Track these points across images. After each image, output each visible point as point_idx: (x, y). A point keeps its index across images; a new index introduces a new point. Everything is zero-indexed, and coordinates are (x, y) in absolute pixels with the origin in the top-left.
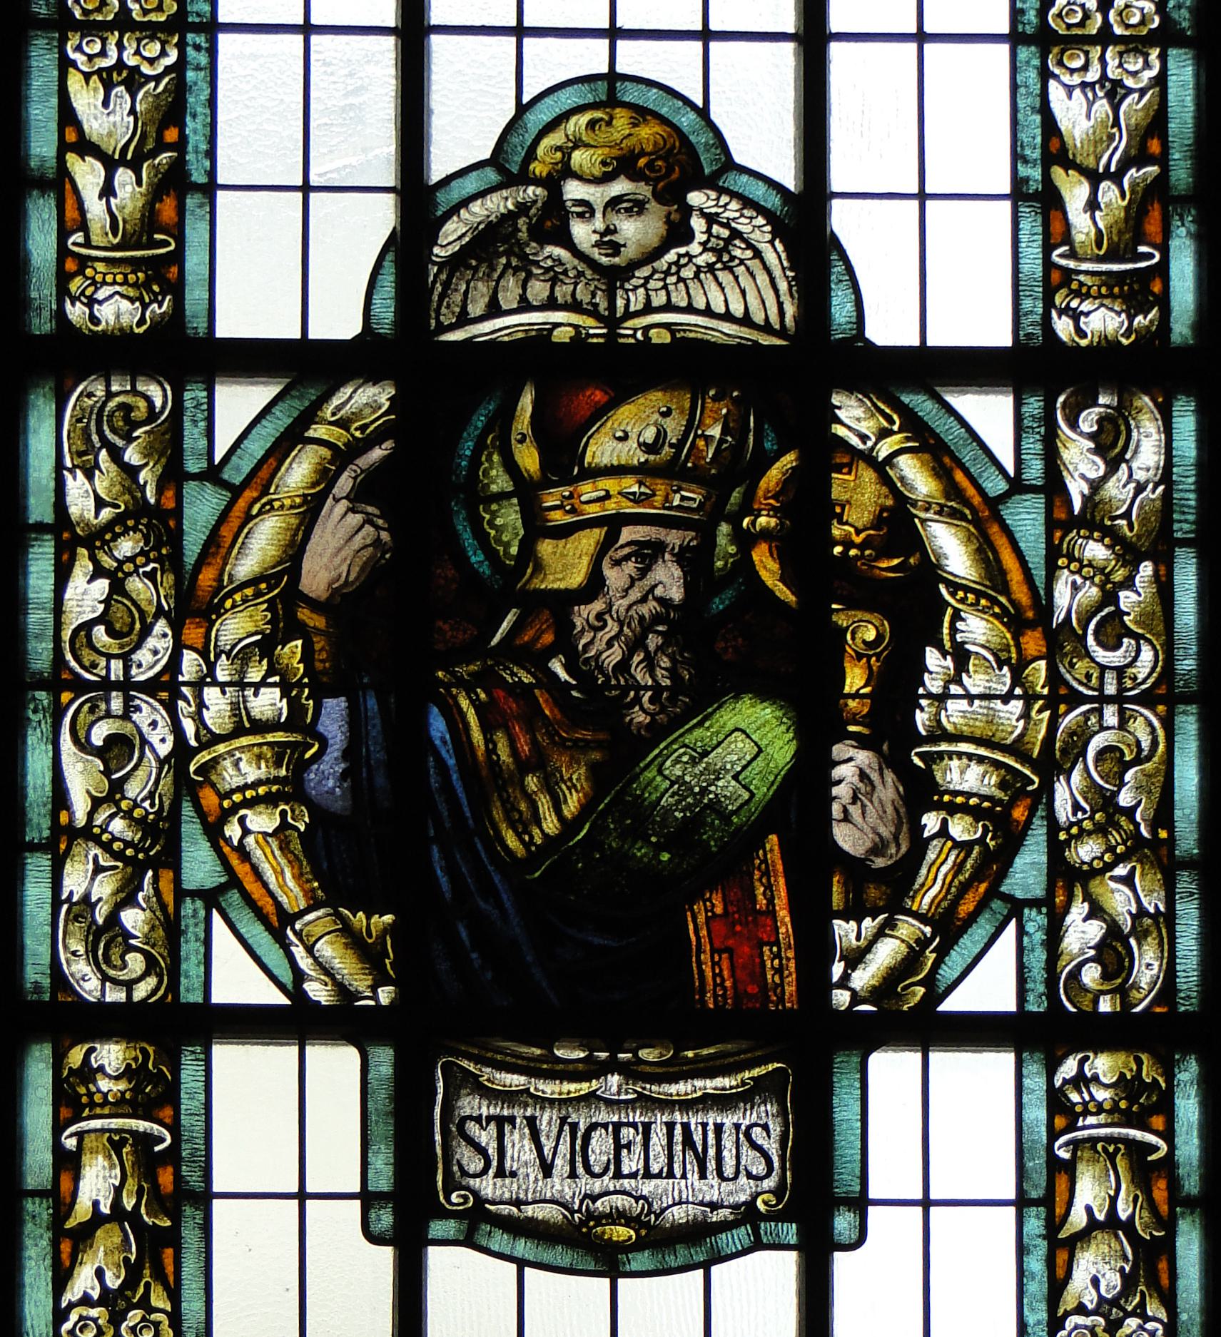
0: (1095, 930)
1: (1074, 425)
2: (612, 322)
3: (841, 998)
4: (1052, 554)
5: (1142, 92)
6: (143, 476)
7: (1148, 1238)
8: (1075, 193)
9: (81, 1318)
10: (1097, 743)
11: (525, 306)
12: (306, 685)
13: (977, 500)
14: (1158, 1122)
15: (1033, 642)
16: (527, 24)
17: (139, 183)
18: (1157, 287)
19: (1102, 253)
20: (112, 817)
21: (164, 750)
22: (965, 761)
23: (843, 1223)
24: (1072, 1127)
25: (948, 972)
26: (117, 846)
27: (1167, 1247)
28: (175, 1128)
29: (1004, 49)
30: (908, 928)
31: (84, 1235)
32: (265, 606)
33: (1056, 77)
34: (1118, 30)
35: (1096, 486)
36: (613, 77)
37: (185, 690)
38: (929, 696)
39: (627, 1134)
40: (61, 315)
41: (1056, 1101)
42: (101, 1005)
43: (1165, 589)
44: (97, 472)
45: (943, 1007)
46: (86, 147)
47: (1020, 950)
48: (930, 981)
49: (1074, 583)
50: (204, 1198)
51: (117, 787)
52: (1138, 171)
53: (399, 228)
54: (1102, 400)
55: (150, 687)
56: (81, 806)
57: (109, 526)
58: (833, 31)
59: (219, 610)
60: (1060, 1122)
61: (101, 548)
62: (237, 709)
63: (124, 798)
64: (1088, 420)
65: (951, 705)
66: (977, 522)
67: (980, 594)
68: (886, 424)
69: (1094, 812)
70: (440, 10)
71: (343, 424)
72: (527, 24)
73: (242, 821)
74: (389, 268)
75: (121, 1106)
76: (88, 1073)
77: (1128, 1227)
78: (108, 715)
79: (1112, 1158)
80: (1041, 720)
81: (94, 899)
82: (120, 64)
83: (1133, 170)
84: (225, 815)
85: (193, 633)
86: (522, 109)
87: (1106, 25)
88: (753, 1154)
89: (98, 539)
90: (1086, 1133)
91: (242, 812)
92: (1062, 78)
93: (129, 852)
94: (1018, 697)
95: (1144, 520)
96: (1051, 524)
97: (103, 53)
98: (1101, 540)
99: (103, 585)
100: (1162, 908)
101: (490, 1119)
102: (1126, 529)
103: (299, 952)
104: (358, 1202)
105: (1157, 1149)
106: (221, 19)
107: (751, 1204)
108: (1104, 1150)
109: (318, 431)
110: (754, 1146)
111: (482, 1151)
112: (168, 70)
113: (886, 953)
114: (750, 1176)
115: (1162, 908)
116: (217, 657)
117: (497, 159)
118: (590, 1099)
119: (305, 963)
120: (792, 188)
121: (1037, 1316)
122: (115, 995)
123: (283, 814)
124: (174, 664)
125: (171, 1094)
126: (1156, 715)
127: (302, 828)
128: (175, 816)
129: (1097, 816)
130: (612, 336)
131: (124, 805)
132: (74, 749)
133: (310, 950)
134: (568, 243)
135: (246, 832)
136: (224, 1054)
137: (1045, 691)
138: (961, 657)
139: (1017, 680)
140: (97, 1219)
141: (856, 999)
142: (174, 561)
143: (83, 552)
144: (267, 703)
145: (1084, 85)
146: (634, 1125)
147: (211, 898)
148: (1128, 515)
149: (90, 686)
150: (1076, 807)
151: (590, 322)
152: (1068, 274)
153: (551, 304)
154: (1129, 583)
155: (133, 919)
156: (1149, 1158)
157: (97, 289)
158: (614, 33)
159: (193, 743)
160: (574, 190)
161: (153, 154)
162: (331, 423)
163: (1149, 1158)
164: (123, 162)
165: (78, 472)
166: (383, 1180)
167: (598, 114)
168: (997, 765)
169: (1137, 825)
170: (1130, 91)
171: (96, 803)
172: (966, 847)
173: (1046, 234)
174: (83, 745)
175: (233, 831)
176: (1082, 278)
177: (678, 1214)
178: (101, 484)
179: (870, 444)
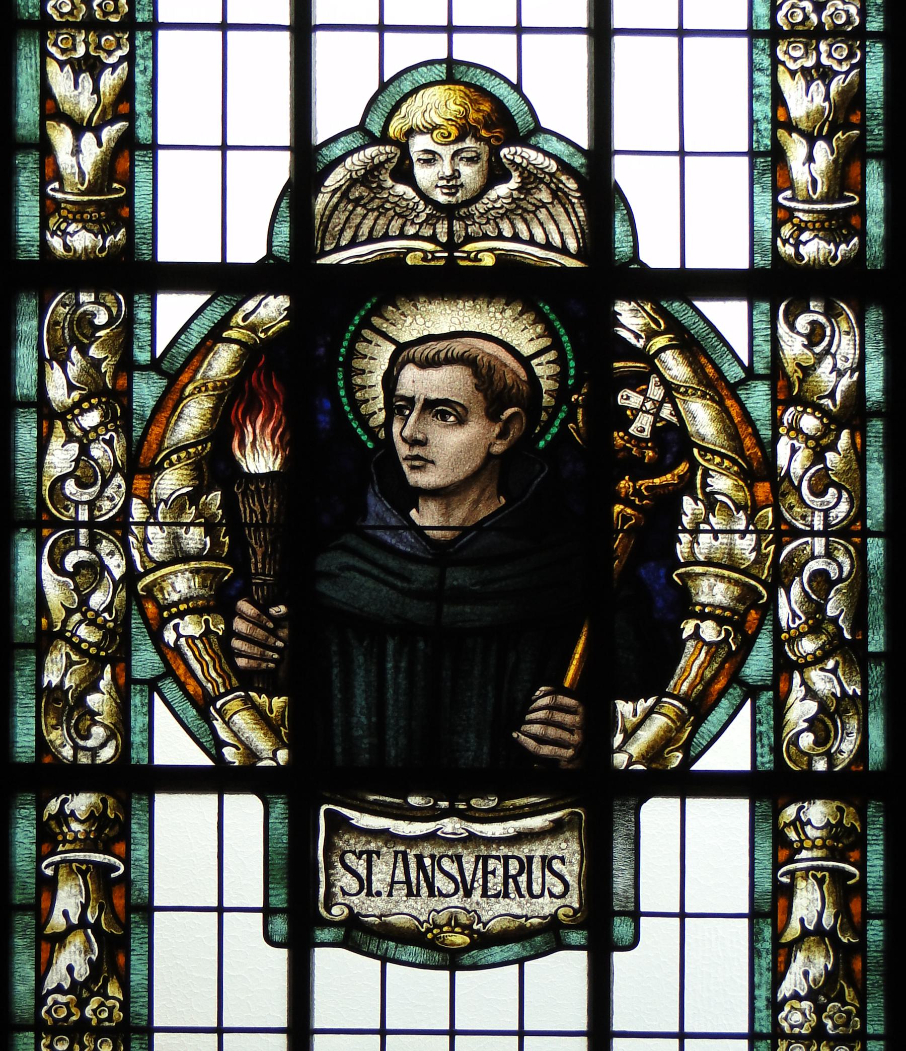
0: (811, 707)
1: (792, 327)
3: (620, 760)
4: (776, 422)
5: (114, 67)
8: (796, 149)
10: (814, 565)
11: (402, 236)
15: (763, 490)
16: (386, 22)
18: (125, 212)
19: (83, 188)
20: (80, 622)
21: (118, 573)
22: (712, 580)
23: (621, 928)
25: (701, 739)
28: (127, 861)
30: (671, 706)
31: (60, 939)
33: (783, 63)
36: (450, 62)
37: (133, 527)
38: (137, 524)
39: (492, 864)
40: (44, 245)
41: (779, 839)
44: (69, 363)
45: (694, 768)
46: (791, 127)
47: (754, 723)
48: (686, 748)
49: (793, 445)
50: (148, 910)
51: (84, 601)
52: (843, 134)
53: (293, 180)
55: (109, 526)
56: (58, 614)
57: (77, 404)
59: (160, 468)
60: (783, 854)
61: (72, 420)
62: (175, 540)
64: (803, 322)
67: (723, 456)
71: (253, 328)
72: (386, 22)
73: (176, 627)
75: (89, 845)
76: (799, 823)
77: (96, 927)
81: (66, 687)
82: (818, 64)
83: (840, 134)
84: (164, 622)
85: (140, 484)
86: (384, 86)
88: (556, 880)
89: (67, 414)
91: (177, 621)
92: (787, 64)
93: (93, 651)
94: (751, 532)
95: (845, 397)
96: (775, 402)
100: (859, 691)
101: (362, 853)
102: (831, 407)
103: (218, 724)
106: (160, 20)
107: (554, 916)
108: (84, 870)
109: (233, 334)
110: (354, 873)
112: (122, 59)
113: (658, 723)
114: (552, 895)
115: (859, 691)
116: (158, 505)
117: (362, 128)
118: (431, 837)
120: (585, 147)
122: (84, 759)
124: (126, 509)
125: (125, 835)
126: (789, 543)
128: (125, 622)
130: (451, 260)
131: (90, 615)
132: (51, 571)
135: (179, 636)
138: (711, 502)
139: (750, 520)
140: (71, 929)
142: (127, 430)
143: (59, 424)
144: (194, 538)
146: (497, 858)
149: (65, 525)
150: (795, 615)
152: (791, 211)
154: (833, 447)
155: (94, 700)
157: (69, 225)
158: (450, 29)
162: (242, 327)
165: (55, 363)
166: (279, 899)
168: (737, 583)
169: (841, 629)
170: (837, 73)
171: (70, 612)
174: (58, 568)
175: (170, 636)
176: (800, 215)
178: (73, 371)
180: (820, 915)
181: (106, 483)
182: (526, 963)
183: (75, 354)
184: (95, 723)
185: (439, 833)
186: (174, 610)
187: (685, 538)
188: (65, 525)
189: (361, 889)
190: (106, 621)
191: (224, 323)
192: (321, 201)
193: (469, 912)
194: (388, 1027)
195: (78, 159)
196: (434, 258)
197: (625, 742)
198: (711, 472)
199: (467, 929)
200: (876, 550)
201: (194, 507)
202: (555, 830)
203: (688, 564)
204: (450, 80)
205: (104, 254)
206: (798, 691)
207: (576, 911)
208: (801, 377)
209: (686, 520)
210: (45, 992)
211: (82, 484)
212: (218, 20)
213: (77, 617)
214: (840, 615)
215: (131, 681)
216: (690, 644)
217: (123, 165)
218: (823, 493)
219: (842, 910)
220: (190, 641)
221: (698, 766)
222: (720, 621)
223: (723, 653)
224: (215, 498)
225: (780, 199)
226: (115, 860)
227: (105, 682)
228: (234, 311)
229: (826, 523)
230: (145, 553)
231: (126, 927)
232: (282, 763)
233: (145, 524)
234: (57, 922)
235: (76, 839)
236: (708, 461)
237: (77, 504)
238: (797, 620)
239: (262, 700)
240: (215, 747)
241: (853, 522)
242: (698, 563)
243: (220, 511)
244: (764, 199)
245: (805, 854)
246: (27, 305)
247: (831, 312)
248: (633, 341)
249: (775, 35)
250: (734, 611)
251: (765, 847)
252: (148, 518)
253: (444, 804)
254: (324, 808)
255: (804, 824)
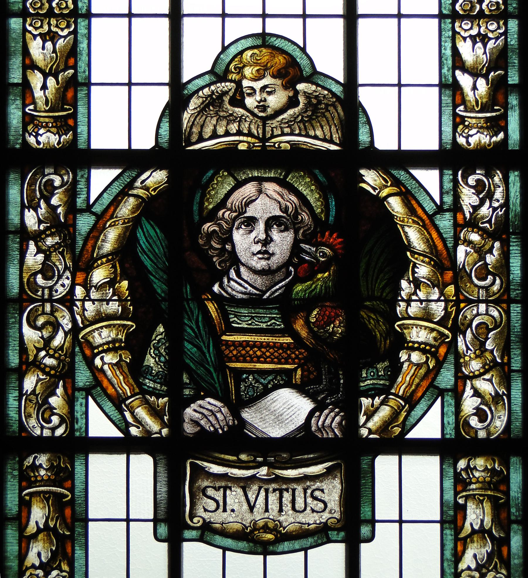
2: (264, 140)
5: (497, 39)
6: (60, 210)
7: (498, 536)
9: (31, 574)
11: (227, 134)
12: (129, 300)
13: (425, 217)
14: (503, 488)
17: (58, 83)
18: (71, 122)
19: (47, 108)
23: (365, 530)
24: (465, 490)
25: (411, 421)
26: (47, 370)
27: (506, 541)
29: (436, 21)
32: (111, 266)
33: (459, 33)
34: (57, 11)
35: (476, 208)
40: (24, 140)
41: (457, 478)
42: (41, 437)
43: (505, 255)
45: (407, 437)
50: (86, 520)
54: (478, 172)
55: (61, 301)
57: (44, 232)
58: (359, 13)
63: (50, 349)
64: (472, 180)
65: (413, 304)
66: (424, 226)
68: (384, 183)
69: (476, 351)
70: (187, 8)
73: (102, 359)
74: (166, 120)
77: (54, 530)
78: (43, 313)
79: (482, 502)
80: (453, 311)
85: (80, 277)
86: (225, 49)
87: (51, 8)
90: (471, 493)
96: (456, 225)
97: (41, 27)
98: (478, 233)
99: (40, 257)
101: (220, 488)
103: (127, 414)
104: (152, 523)
105: (68, 496)
107: (326, 523)
108: (46, 497)
111: (217, 502)
113: (385, 412)
117: (212, 72)
119: (130, 419)
120: (343, 82)
121: (449, 570)
122: (47, 433)
123: (120, 356)
124: (72, 291)
125: (71, 476)
127: (128, 361)
128: (73, 355)
129: (477, 352)
130: (264, 147)
133: (132, 413)
134: (245, 107)
135: (104, 363)
136: (93, 458)
137: (454, 298)
139: (442, 293)
141: (370, 432)
145: (471, 36)
147: (88, 391)
148: (489, 222)
151: (253, 140)
152: (463, 118)
153: (239, 133)
154: (490, 251)
156: (64, 500)
157: (39, 129)
158: (264, 16)
159: (81, 325)
160: (246, 83)
161: (64, 70)
163: (64, 500)
164: (50, 74)
167: (256, 51)
170: (490, 39)
172: (419, 366)
173: (454, 101)
175: (98, 362)
177: (291, 528)
179: (377, 191)
180: (482, 521)
181: (60, 277)
182: (309, 551)
183: (43, 204)
184: (54, 414)
185: (257, 475)
186: (100, 349)
187: (403, 304)
188: (37, 301)
189: (218, 508)
190: (60, 355)
191: (130, 185)
192: (186, 116)
193: (275, 521)
194: (131, 517)
195: (44, 93)
196: (254, 146)
197: (367, 420)
198: (417, 265)
199: (274, 530)
200: (516, 309)
201: (112, 289)
202: (329, 472)
203: (404, 318)
204: (264, 45)
205: (60, 145)
206: (469, 392)
207: (339, 521)
208: (471, 211)
209: (404, 294)
210: (24, 568)
211: (45, 278)
212: (301, 13)
213: (43, 353)
214: (494, 348)
215: (75, 389)
216: (406, 365)
217: (70, 94)
218: (485, 279)
219: (496, 519)
220: (110, 366)
221: (410, 436)
222: (424, 351)
223: (422, 371)
224: (125, 284)
225: (457, 111)
226: (64, 490)
227: (60, 391)
228: (134, 179)
229: (488, 295)
230: (83, 316)
231: (72, 529)
232: (164, 436)
233: (83, 301)
234: (32, 528)
235: (43, 480)
236: (416, 259)
237: (43, 288)
238: (469, 351)
239: (152, 399)
240: (124, 427)
241: (502, 295)
242: (410, 318)
243: (128, 292)
244: (448, 111)
245: (473, 486)
246: (13, 177)
247: (489, 175)
248: (372, 191)
249: (454, 16)
250: (431, 346)
251: (449, 484)
252: (85, 297)
253: (260, 459)
254: (189, 461)
255: (472, 470)
